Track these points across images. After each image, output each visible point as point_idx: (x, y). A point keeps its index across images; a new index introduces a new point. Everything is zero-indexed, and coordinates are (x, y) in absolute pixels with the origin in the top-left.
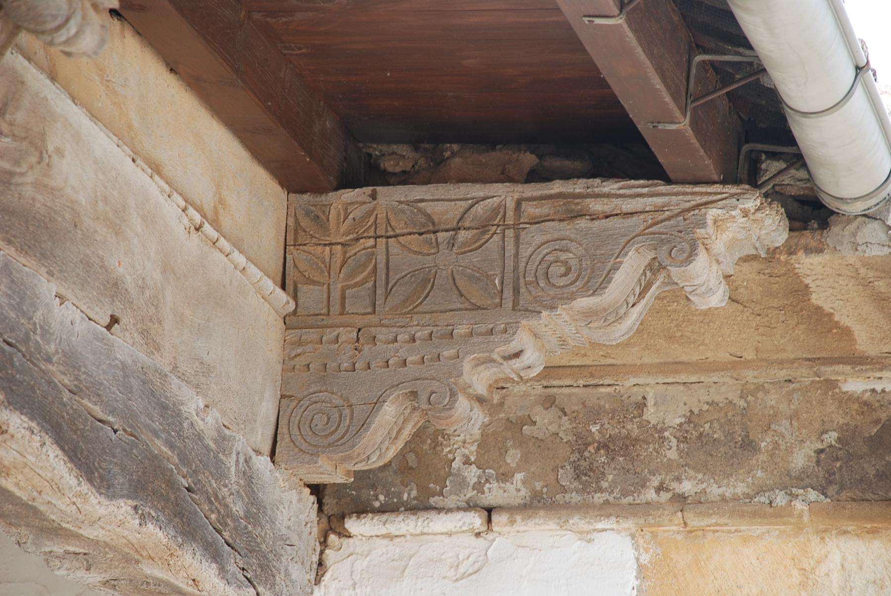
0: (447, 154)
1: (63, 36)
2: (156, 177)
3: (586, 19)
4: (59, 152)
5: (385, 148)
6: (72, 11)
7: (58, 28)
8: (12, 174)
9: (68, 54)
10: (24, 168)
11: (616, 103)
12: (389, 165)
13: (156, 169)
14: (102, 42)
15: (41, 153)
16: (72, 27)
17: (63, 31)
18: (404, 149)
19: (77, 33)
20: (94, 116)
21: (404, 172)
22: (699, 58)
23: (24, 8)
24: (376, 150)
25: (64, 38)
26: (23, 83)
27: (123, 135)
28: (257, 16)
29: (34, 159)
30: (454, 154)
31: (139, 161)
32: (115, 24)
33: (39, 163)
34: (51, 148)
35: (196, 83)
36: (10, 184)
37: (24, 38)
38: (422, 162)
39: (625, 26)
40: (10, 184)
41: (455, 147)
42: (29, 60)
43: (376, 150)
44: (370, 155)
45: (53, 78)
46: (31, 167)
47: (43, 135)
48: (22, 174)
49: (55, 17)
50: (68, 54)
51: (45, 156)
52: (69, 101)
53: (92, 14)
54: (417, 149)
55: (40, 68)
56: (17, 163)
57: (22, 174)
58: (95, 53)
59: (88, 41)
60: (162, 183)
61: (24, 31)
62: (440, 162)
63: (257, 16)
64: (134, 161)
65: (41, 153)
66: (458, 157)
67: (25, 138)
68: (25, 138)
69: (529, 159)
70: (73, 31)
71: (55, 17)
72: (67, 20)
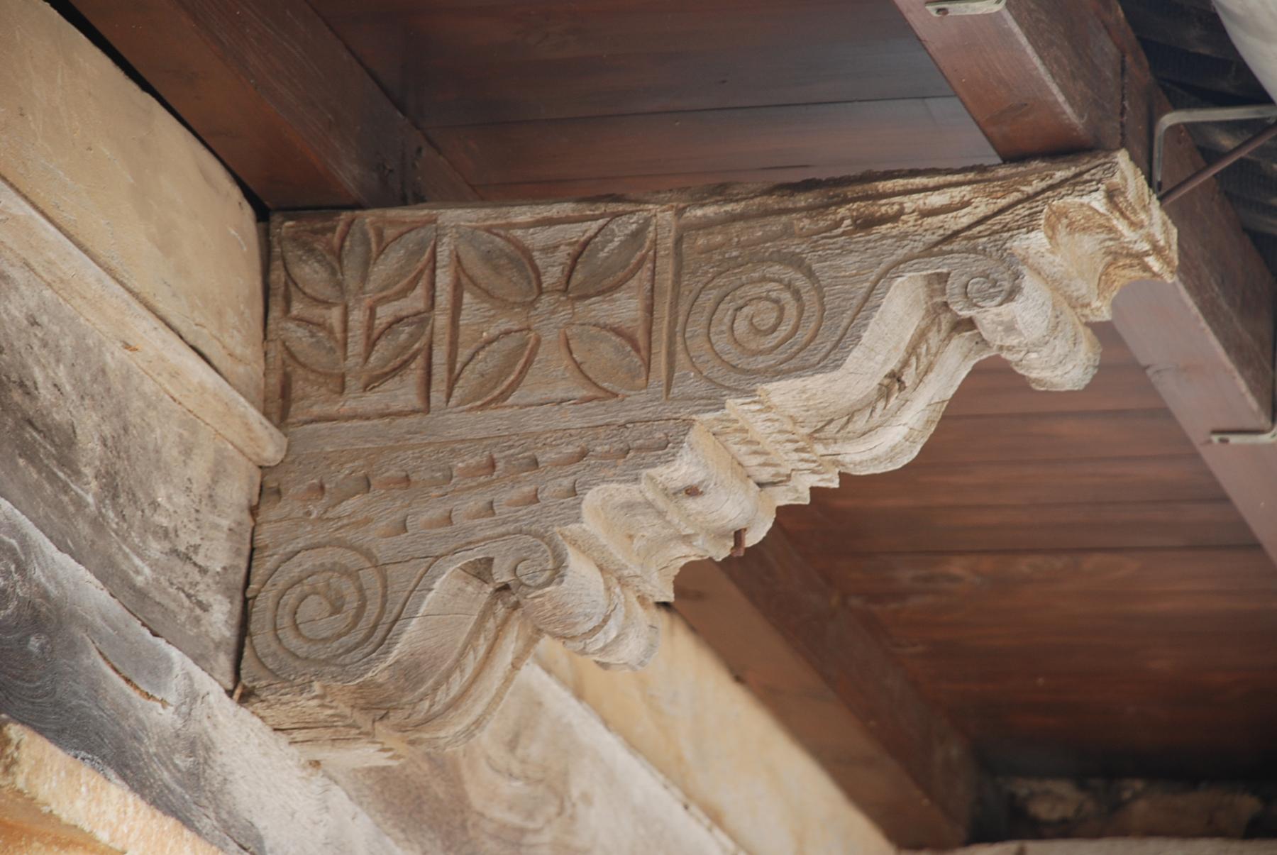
0: (1127, 795)
1: (599, 641)
2: (717, 831)
3: (1215, 438)
4: (587, 798)
5: (1035, 785)
6: (612, 607)
7: (594, 631)
8: (523, 831)
9: (605, 666)
10: (539, 822)
11: (1210, 474)
12: (1042, 810)
13: (716, 818)
14: (652, 647)
15: (562, 803)
16: (612, 630)
17: (600, 635)
18: (1063, 788)
19: (618, 637)
20: (633, 746)
21: (1064, 821)
22: (1170, 119)
23: (548, 606)
24: (1022, 788)
25: (601, 645)
26: (540, 704)
27: (671, 771)
28: (855, 602)
29: (552, 810)
30: (1136, 796)
31: (693, 808)
32: (662, 618)
33: (559, 814)
34: (575, 793)
35: (772, 698)
36: (520, 845)
37: (546, 644)
38: (1090, 806)
39: (1008, 16)
40: (520, 845)
41: (1139, 785)
42: (549, 671)
43: (1022, 788)
44: (1013, 796)
45: (579, 695)
46: (549, 821)
47: (565, 775)
48: (537, 831)
49: (589, 617)
50: (605, 666)
51: (568, 805)
52: (600, 727)
53: (638, 610)
54: (1082, 786)
55: (563, 682)
56: (530, 815)
57: (537, 831)
58: (641, 663)
59: (632, 649)
60: (724, 839)
61: (547, 637)
62: (1117, 806)
63: (855, 602)
64: (686, 807)
65: (562, 798)
66: (1142, 800)
67: (541, 781)
68: (541, 781)
69: (1248, 804)
70: (613, 635)
71: (589, 617)
72: (605, 621)
